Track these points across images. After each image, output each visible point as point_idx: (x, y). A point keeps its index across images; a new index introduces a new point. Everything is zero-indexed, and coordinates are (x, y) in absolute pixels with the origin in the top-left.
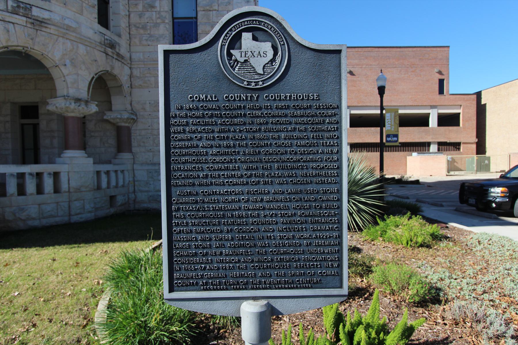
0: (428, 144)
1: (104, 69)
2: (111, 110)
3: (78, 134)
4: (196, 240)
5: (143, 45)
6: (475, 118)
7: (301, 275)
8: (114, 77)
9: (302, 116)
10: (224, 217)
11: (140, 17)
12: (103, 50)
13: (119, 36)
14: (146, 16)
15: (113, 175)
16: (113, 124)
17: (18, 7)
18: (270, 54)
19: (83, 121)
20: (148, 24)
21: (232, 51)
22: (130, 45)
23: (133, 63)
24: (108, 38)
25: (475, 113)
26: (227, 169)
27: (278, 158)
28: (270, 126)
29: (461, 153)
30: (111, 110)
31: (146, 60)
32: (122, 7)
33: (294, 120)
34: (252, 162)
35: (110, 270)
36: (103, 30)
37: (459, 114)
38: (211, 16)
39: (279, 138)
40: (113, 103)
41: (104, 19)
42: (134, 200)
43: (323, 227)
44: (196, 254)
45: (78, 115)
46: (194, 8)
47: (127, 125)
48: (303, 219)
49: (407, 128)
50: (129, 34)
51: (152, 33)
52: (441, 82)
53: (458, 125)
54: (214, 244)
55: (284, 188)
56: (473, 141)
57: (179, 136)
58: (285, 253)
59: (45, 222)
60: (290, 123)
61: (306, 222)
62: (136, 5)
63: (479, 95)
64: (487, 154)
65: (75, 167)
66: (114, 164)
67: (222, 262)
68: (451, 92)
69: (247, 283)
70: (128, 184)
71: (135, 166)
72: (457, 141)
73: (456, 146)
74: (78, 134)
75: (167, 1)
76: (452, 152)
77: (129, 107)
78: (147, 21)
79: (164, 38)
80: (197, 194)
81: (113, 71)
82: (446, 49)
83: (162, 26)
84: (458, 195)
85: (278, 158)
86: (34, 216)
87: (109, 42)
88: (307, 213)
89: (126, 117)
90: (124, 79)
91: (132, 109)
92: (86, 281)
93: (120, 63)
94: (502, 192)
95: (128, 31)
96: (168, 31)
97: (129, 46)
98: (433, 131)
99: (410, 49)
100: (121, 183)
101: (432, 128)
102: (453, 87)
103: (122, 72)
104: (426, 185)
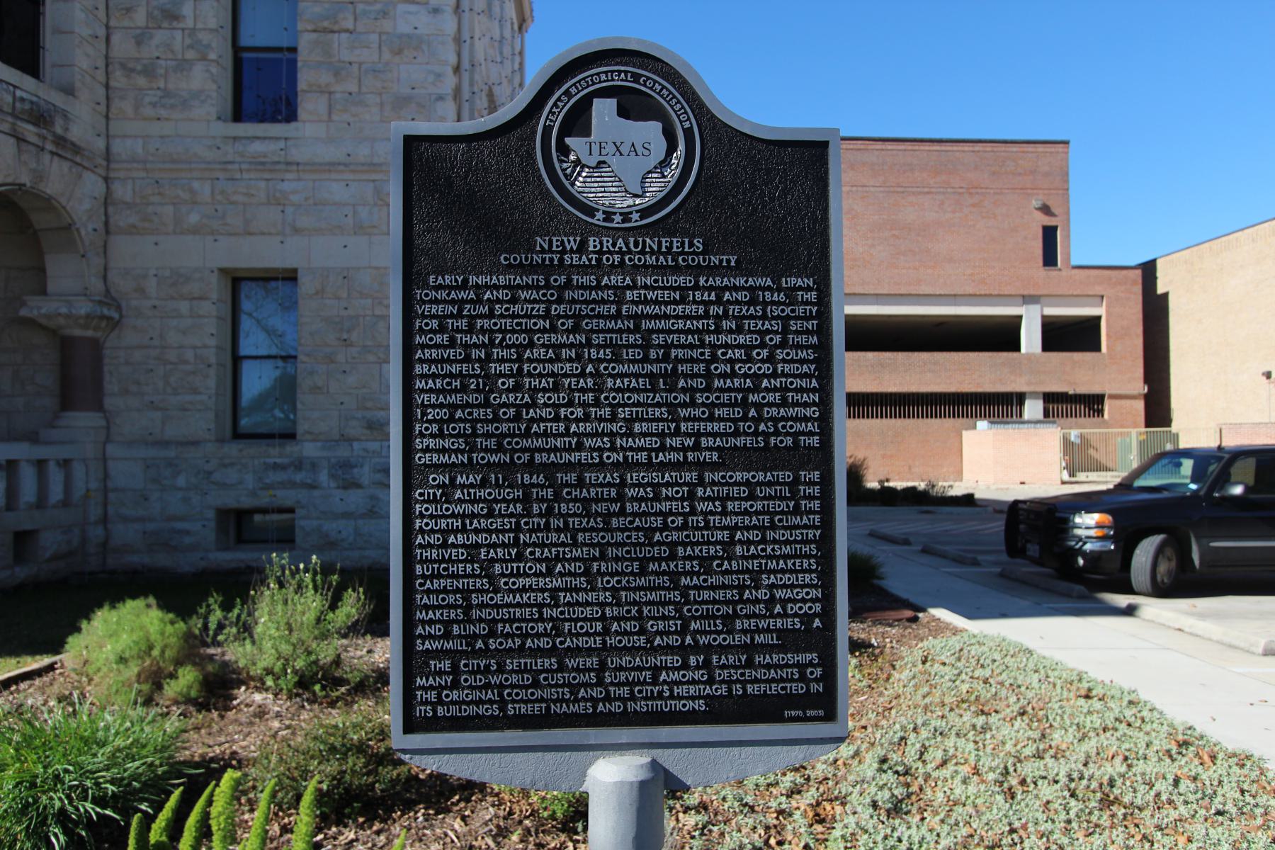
0: (1020, 398)
1: (10, 180)
2: (43, 292)
5: (145, 119)
6: (1139, 330)
11: (139, 42)
13: (69, 91)
14: (156, 41)
16: (53, 332)
18: (660, 145)
20: (161, 62)
21: (568, 140)
22: (107, 117)
23: (113, 166)
24: (25, 95)
25: (1141, 316)
29: (1105, 421)
30: (43, 292)
31: (151, 158)
32: (79, 15)
37: (1099, 318)
38: (336, 45)
40: (49, 272)
42: (105, 544)
47: (89, 333)
49: (966, 354)
50: (107, 86)
51: (171, 86)
52: (1049, 234)
53: (1096, 347)
56: (1135, 392)
62: (128, 10)
63: (1149, 270)
64: (1175, 427)
68: (1074, 262)
70: (86, 497)
71: (111, 450)
72: (1095, 390)
73: (1093, 404)
75: (215, 4)
76: (1082, 420)
77: (97, 285)
78: (157, 54)
79: (203, 102)
81: (41, 186)
82: (1060, 148)
83: (198, 69)
84: (1003, 534)
87: (27, 106)
89: (83, 312)
91: (108, 291)
93: (66, 165)
94: (1099, 526)
95: (102, 78)
96: (214, 81)
97: (104, 121)
98: (1031, 366)
99: (967, 147)
101: (1029, 356)
102: (1080, 247)
104: (990, 509)
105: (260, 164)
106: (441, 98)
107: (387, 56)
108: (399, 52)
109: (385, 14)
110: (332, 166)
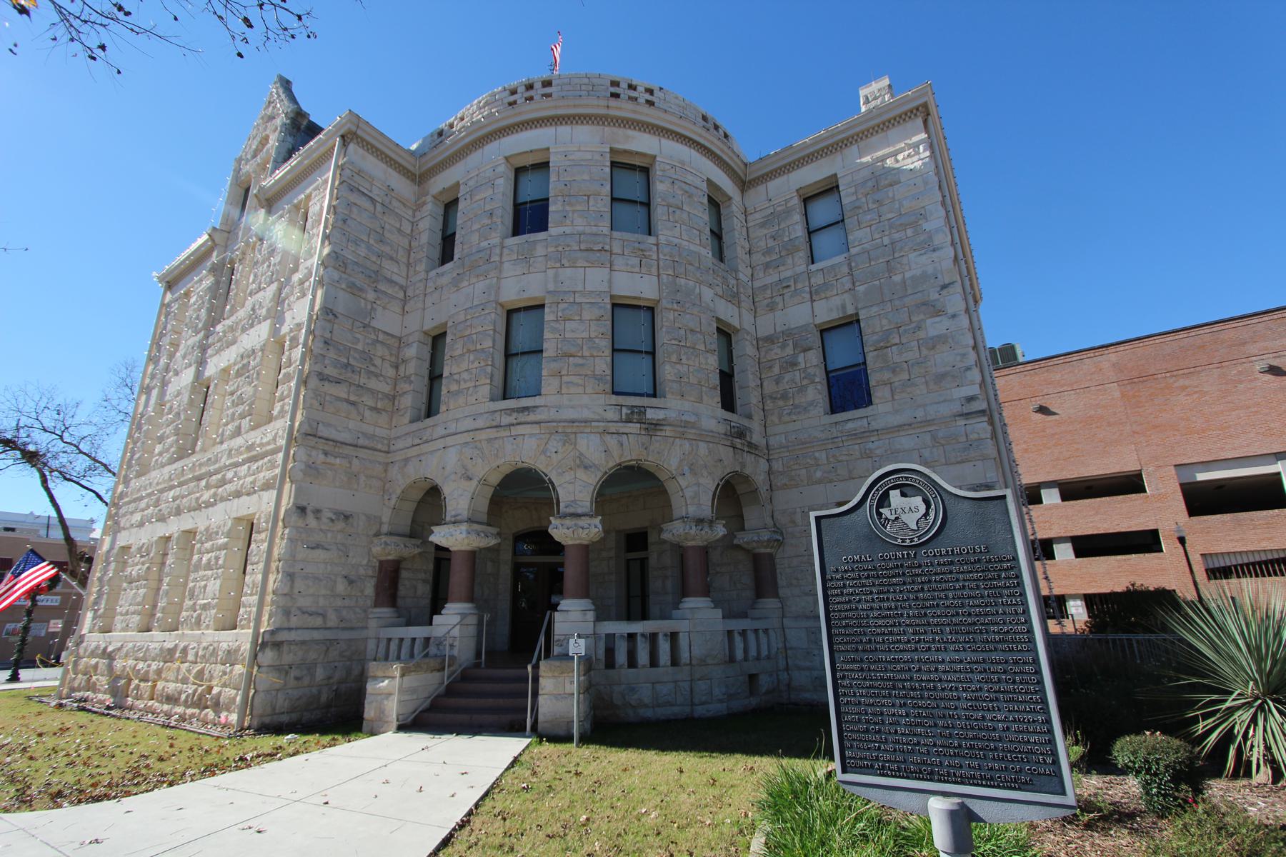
2: (743, 529)
3: (695, 572)
4: (866, 714)
7: (1001, 770)
8: (746, 479)
9: (970, 572)
10: (894, 688)
12: (728, 443)
13: (750, 417)
15: (751, 637)
17: (632, 413)
19: (705, 551)
26: (891, 633)
27: (948, 620)
28: (934, 585)
30: (743, 529)
32: (751, 377)
33: (961, 576)
34: (918, 625)
35: (765, 796)
36: (728, 415)
39: (947, 597)
41: (728, 402)
42: (789, 685)
43: (1022, 707)
44: (867, 731)
45: (701, 544)
46: (860, 350)
47: (768, 550)
48: (993, 696)
54: (888, 720)
55: (962, 655)
57: (838, 599)
58: (975, 738)
59: (663, 712)
60: (957, 580)
61: (997, 699)
65: (698, 622)
66: (753, 619)
67: (898, 742)
69: (932, 773)
74: (695, 572)
77: (769, 521)
80: (862, 661)
85: (948, 620)
86: (647, 701)
88: (996, 687)
90: (760, 479)
92: (728, 810)
100: (764, 653)
103: (756, 470)
105: (854, 435)
106: (968, 369)
107: (925, 352)
108: (933, 347)
109: (919, 328)
110: (900, 427)
